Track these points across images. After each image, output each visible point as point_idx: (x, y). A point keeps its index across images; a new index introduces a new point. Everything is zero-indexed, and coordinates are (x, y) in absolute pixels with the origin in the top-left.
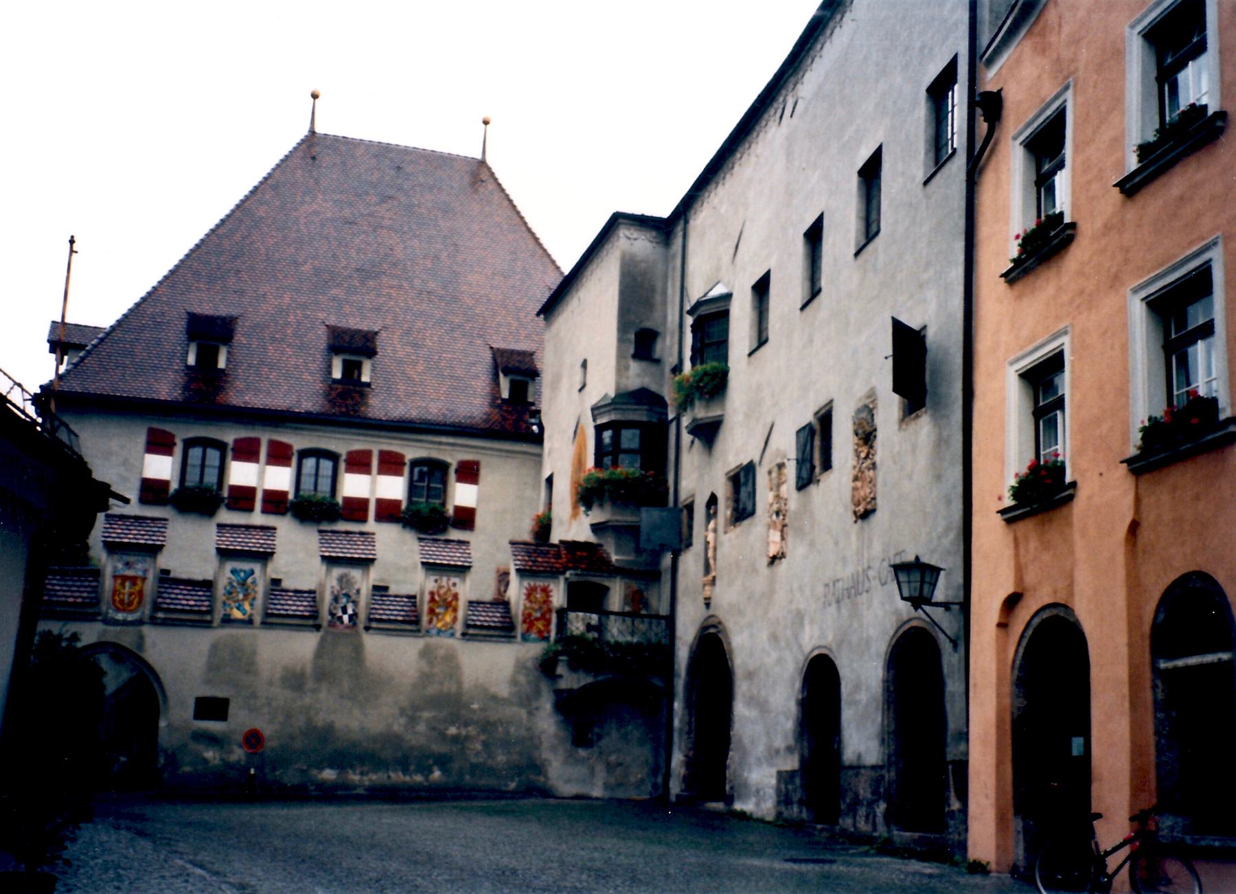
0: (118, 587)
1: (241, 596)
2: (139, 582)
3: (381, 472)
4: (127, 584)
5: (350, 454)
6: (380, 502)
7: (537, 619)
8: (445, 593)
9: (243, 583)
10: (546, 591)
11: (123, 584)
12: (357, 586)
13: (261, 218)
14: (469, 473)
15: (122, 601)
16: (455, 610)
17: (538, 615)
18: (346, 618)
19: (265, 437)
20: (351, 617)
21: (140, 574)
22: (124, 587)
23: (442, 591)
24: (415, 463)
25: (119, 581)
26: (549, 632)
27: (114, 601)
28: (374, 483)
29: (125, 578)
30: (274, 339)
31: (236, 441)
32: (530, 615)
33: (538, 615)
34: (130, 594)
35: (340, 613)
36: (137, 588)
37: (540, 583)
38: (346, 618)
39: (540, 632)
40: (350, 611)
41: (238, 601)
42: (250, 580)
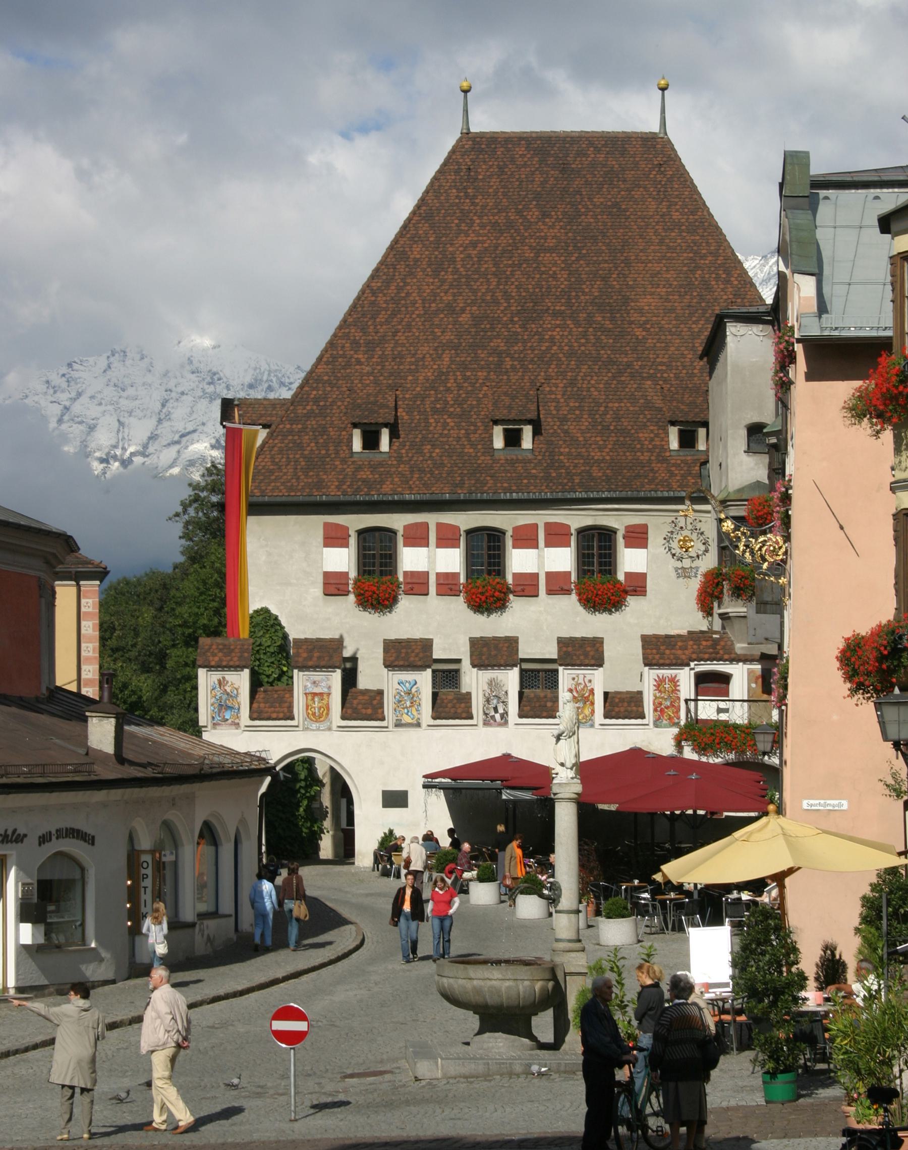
0: (310, 702)
1: (408, 704)
2: (325, 697)
3: (548, 545)
4: (316, 699)
5: (516, 529)
6: (548, 574)
7: (667, 708)
8: (583, 690)
9: (409, 693)
10: (674, 681)
11: (313, 699)
12: (505, 689)
13: (416, 261)
14: (638, 537)
15: (314, 714)
16: (592, 704)
17: (668, 703)
18: (498, 716)
19: (432, 519)
20: (502, 716)
21: (326, 690)
22: (314, 702)
23: (579, 688)
24: (581, 531)
25: (310, 697)
26: (679, 718)
27: (308, 714)
28: (541, 558)
29: (315, 694)
30: (435, 411)
31: (406, 528)
32: (660, 704)
33: (668, 703)
34: (320, 708)
35: (492, 713)
36: (325, 702)
37: (667, 672)
38: (498, 716)
39: (670, 718)
40: (501, 711)
41: (407, 707)
42: (414, 690)
